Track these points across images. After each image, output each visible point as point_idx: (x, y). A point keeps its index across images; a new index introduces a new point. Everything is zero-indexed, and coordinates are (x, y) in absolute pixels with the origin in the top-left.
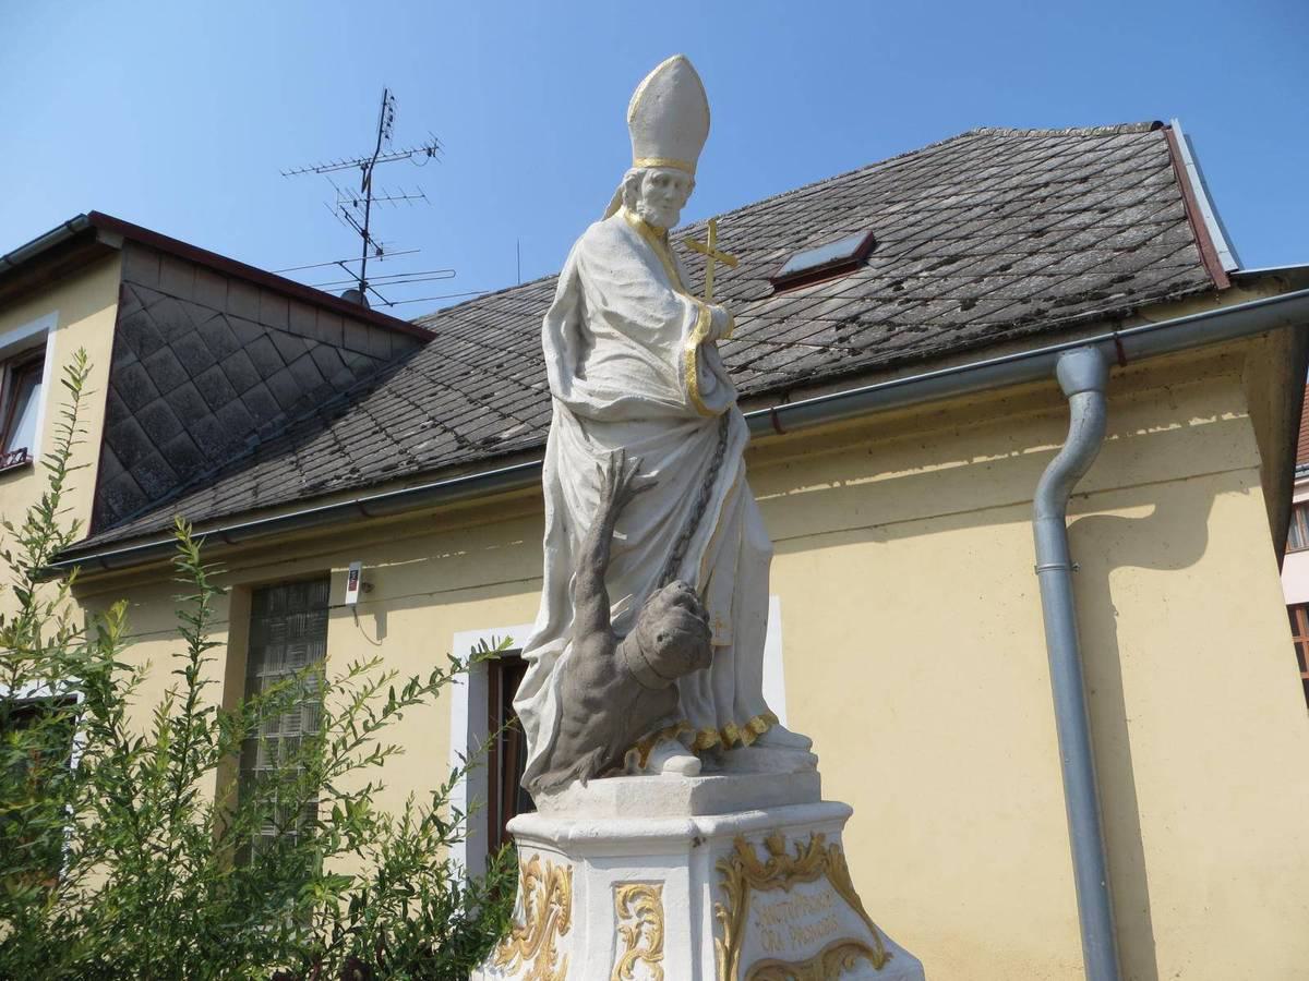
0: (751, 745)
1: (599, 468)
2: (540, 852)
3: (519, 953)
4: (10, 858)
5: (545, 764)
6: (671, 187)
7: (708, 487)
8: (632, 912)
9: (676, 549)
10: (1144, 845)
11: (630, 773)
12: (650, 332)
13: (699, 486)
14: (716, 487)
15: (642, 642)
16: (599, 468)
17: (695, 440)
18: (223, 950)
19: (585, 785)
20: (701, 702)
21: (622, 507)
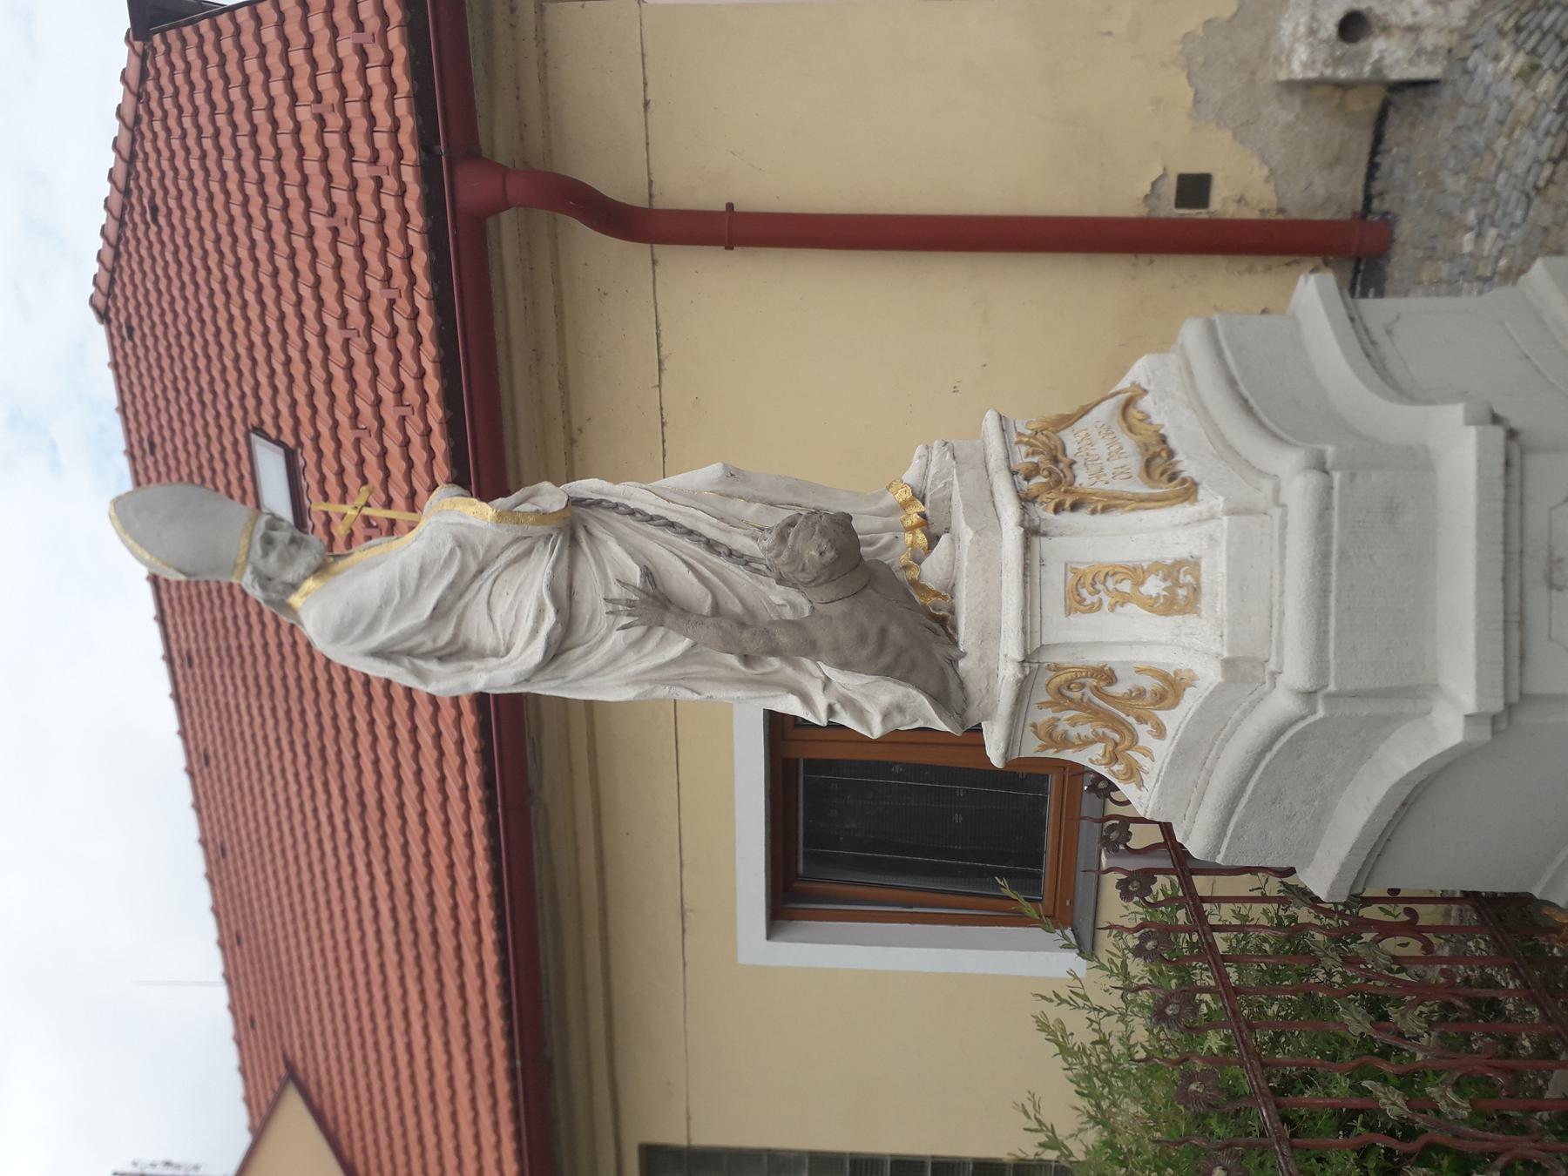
0: (924, 504)
1: (624, 628)
2: (1029, 721)
3: (1129, 752)
4: (1161, 898)
5: (941, 700)
6: (275, 534)
7: (651, 519)
8: (1095, 599)
9: (719, 554)
10: (208, 930)
11: (952, 611)
12: (462, 571)
13: (650, 529)
14: (651, 511)
15: (822, 579)
16: (624, 628)
17: (597, 530)
18: (1314, 3)
19: (964, 655)
20: (878, 545)
21: (670, 602)
